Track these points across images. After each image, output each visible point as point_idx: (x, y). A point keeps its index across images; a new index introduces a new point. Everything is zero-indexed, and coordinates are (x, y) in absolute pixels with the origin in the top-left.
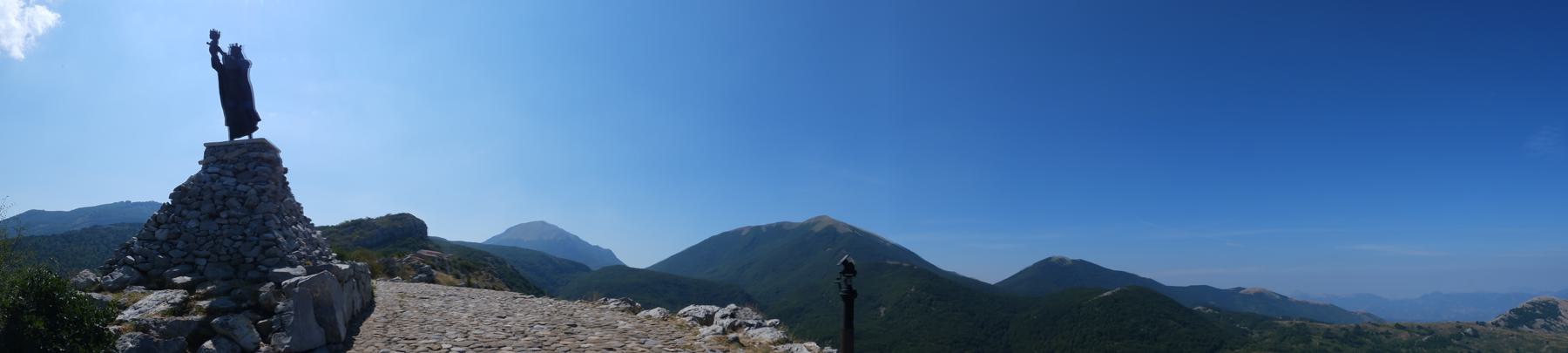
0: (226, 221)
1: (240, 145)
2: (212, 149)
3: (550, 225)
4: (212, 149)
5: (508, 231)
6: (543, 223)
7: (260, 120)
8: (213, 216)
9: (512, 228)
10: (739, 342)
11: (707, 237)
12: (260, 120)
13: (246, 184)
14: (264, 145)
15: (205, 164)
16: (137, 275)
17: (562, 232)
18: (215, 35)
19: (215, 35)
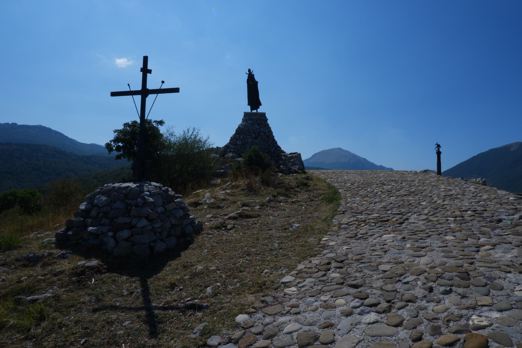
0: (261, 140)
1: (254, 113)
2: (246, 114)
3: (345, 151)
4: (246, 114)
5: (314, 156)
6: (340, 149)
7: (261, 105)
8: (256, 138)
9: (316, 154)
10: (472, 308)
11: (475, 154)
12: (261, 105)
13: (263, 128)
14: (263, 115)
15: (244, 120)
16: (237, 155)
17: (354, 156)
18: (246, 73)
19: (246, 73)
